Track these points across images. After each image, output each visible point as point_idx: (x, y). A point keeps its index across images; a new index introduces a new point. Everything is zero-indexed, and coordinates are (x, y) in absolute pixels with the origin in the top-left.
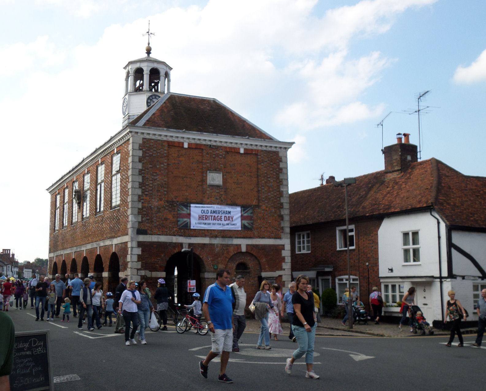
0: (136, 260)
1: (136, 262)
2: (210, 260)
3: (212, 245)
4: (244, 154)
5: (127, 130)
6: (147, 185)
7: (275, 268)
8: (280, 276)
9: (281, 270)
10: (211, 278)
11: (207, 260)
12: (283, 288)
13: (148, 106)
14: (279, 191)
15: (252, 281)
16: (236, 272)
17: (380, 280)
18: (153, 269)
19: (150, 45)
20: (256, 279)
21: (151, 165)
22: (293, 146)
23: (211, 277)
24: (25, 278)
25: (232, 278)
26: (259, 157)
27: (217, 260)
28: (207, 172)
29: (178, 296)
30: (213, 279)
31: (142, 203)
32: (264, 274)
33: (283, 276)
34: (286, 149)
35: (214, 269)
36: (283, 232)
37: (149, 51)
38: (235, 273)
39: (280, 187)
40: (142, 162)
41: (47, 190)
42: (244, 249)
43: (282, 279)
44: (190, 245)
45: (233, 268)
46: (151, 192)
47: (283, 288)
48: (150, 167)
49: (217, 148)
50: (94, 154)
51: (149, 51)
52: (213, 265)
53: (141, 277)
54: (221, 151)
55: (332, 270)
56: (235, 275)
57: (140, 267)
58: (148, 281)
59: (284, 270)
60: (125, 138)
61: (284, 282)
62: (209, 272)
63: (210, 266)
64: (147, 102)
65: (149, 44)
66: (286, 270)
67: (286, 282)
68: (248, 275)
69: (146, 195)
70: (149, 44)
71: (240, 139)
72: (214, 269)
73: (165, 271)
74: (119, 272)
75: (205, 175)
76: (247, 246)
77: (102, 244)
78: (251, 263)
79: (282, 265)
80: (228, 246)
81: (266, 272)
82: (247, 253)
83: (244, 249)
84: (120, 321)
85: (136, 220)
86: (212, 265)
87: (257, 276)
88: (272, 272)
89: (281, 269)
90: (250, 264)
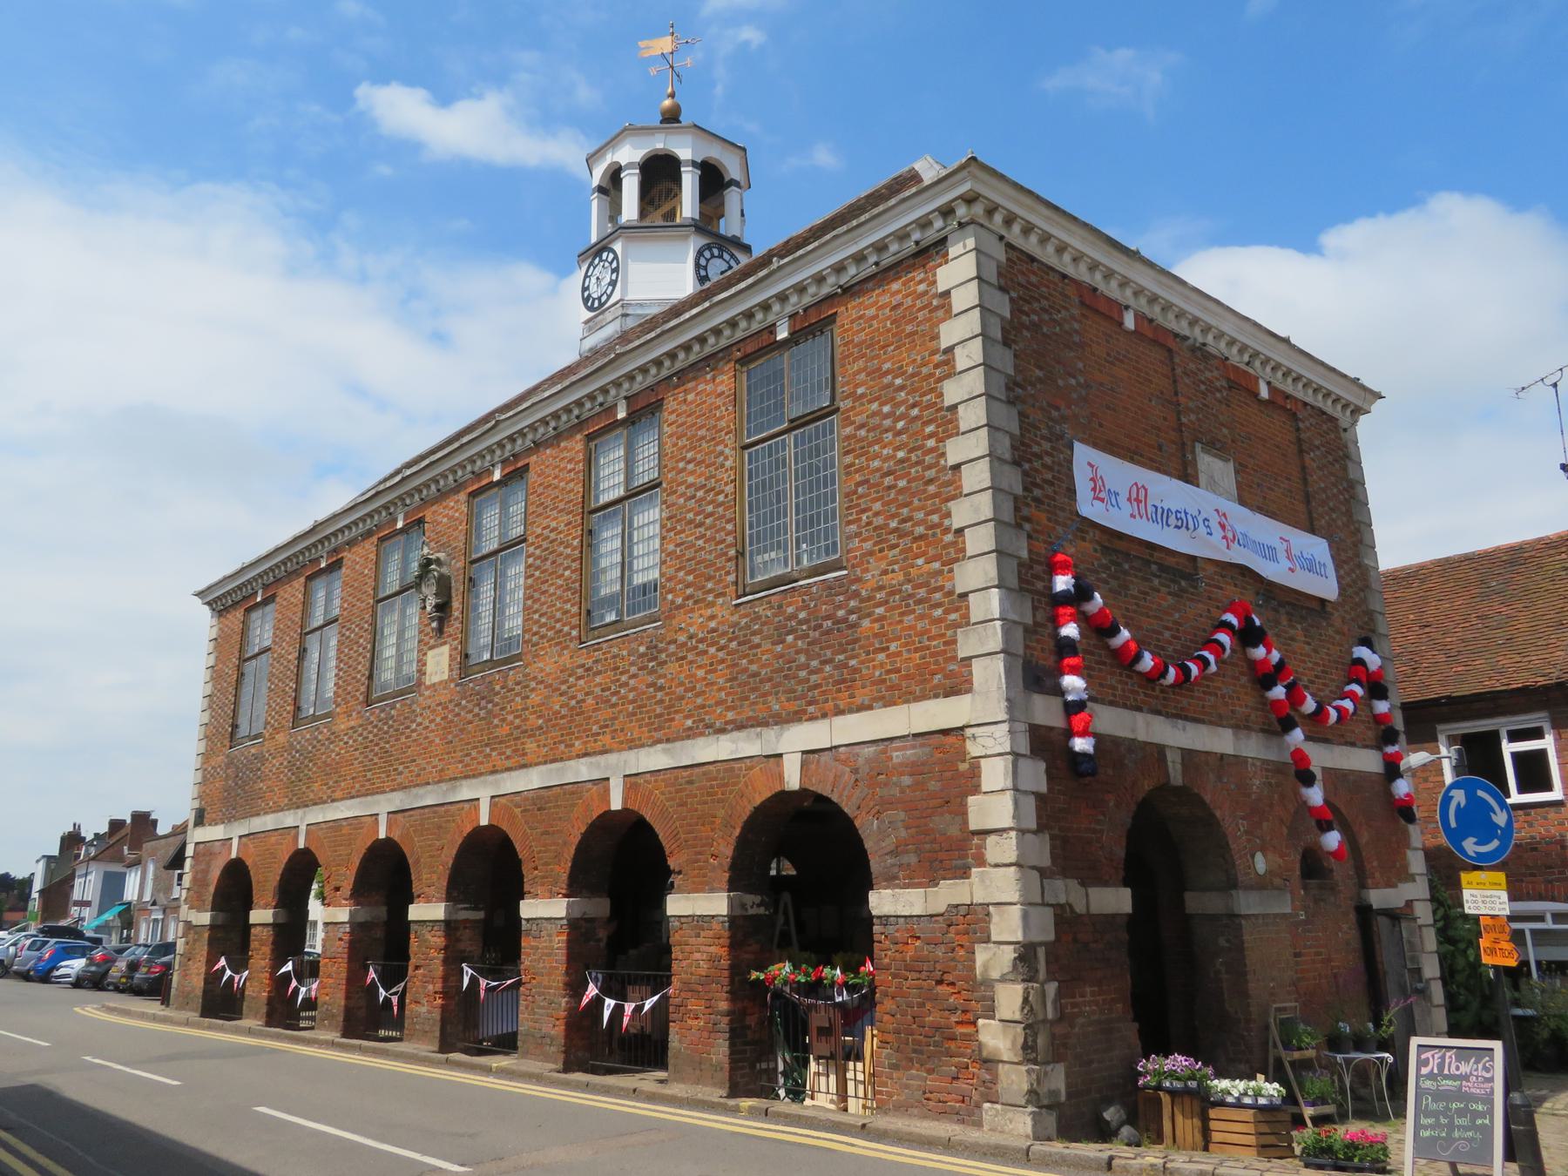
0: (1034, 826)
1: (1035, 832)
3: (1239, 760)
4: (1270, 403)
5: (963, 181)
6: (1038, 456)
13: (702, 279)
14: (1359, 566)
18: (1090, 876)
20: (1352, 916)
21: (1041, 368)
22: (1377, 406)
26: (1301, 425)
28: (1194, 447)
31: (1029, 537)
34: (1358, 411)
40: (1013, 346)
41: (199, 594)
46: (1049, 490)
48: (1040, 380)
50: (584, 386)
54: (1216, 373)
57: (1046, 861)
60: (350, 533)
64: (697, 266)
66: (1417, 878)
69: (1036, 500)
73: (1126, 885)
75: (1190, 457)
77: (654, 759)
84: (1457, 1083)
85: (1016, 618)
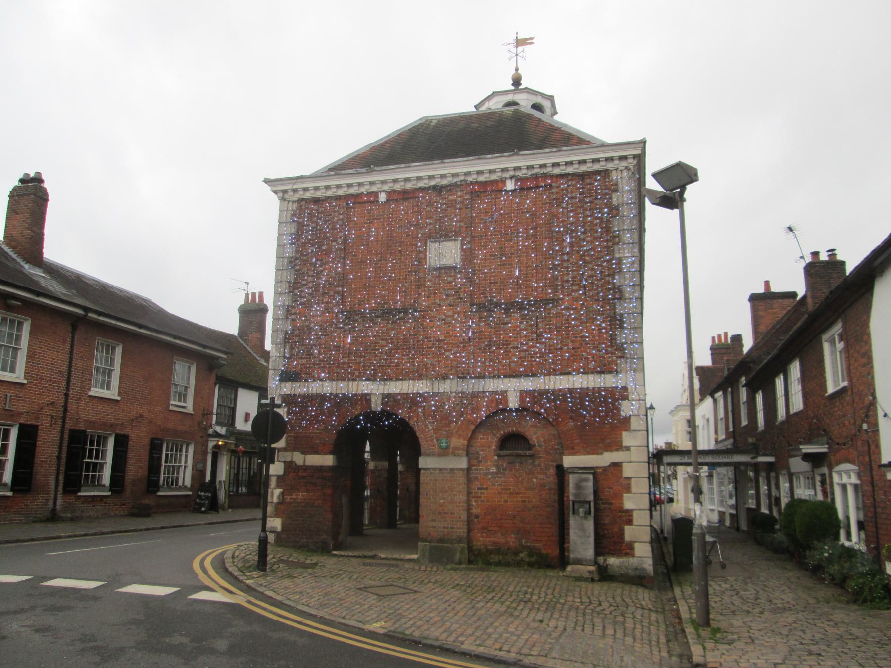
2: (430, 427)
7: (601, 445)
8: (617, 465)
9: (617, 450)
10: (434, 469)
11: (425, 431)
12: (625, 495)
15: (541, 476)
16: (499, 456)
17: (884, 475)
19: (519, 72)
23: (433, 467)
24: (271, 465)
25: (489, 469)
27: (448, 429)
29: (397, 506)
30: (437, 471)
32: (569, 461)
33: (624, 464)
35: (440, 447)
36: (621, 357)
37: (517, 82)
38: (496, 458)
39: (613, 251)
42: (513, 403)
43: (621, 471)
44: (386, 397)
45: (489, 447)
47: (625, 495)
49: (450, 188)
51: (517, 82)
52: (437, 440)
53: (285, 465)
55: (825, 450)
56: (496, 461)
58: (300, 473)
59: (628, 449)
61: (629, 479)
62: (428, 455)
63: (432, 441)
65: (517, 70)
67: (633, 480)
68: (530, 461)
70: (517, 70)
71: (496, 160)
72: (440, 447)
73: (331, 453)
74: (420, 455)
76: (523, 394)
78: (535, 433)
79: (621, 435)
80: (475, 396)
81: (574, 454)
82: (522, 410)
83: (513, 403)
86: (434, 441)
87: (555, 464)
88: (593, 454)
89: (618, 446)
90: (534, 437)
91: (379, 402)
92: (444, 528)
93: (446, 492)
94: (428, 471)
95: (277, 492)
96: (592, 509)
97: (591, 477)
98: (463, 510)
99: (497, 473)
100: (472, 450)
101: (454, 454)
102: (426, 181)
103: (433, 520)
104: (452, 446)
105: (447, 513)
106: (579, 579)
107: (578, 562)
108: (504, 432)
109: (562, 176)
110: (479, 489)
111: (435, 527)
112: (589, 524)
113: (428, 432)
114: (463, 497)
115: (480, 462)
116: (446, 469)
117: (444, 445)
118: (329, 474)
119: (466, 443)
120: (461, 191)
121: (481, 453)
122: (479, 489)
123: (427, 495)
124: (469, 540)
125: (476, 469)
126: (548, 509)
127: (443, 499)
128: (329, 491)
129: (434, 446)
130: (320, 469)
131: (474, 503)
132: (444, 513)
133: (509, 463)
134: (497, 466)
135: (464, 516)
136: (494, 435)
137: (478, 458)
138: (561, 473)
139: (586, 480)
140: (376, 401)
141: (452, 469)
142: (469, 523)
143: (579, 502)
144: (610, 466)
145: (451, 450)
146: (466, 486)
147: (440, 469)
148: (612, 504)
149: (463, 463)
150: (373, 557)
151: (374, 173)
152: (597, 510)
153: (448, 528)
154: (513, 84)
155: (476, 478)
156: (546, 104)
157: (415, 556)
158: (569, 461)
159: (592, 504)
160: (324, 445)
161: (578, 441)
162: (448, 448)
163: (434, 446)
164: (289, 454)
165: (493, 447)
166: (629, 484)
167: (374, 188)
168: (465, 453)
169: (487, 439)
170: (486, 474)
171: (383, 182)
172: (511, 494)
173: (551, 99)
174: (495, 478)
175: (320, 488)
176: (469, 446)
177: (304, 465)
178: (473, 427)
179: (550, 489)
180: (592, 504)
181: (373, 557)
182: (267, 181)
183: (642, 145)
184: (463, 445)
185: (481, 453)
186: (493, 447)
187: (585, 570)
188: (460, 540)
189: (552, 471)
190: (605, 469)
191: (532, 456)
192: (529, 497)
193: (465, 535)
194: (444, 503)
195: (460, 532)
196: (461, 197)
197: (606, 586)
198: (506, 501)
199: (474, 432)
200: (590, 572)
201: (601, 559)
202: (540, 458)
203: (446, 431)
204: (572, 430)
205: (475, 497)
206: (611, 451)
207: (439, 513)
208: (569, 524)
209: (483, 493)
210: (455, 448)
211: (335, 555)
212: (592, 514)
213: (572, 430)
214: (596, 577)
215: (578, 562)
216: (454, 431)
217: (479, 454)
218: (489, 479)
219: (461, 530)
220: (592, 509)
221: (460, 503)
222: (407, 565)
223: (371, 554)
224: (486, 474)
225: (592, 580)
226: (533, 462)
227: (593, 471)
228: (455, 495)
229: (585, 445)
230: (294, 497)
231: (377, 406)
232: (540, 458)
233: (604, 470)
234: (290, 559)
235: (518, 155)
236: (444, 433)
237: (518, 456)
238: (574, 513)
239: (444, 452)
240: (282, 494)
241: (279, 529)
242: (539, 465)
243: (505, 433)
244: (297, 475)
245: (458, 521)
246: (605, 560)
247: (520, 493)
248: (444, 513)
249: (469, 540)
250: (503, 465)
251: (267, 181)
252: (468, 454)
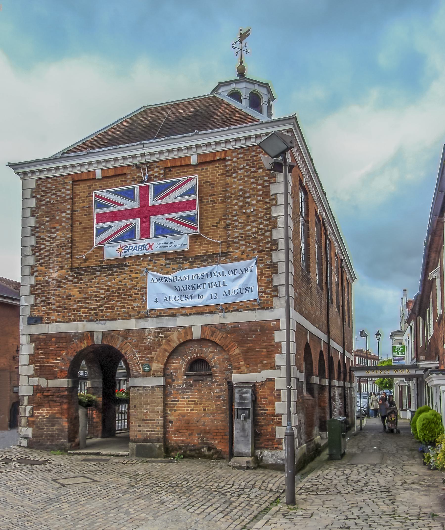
2: (137, 356)
8: (272, 380)
9: (271, 369)
10: (140, 387)
15: (217, 390)
32: (237, 378)
35: (144, 370)
37: (241, 73)
38: (185, 377)
45: (181, 369)
51: (241, 73)
52: (142, 365)
56: (185, 380)
62: (135, 377)
65: (241, 63)
68: (209, 379)
70: (241, 63)
76: (203, 327)
80: (168, 330)
86: (140, 365)
90: (212, 360)
91: (100, 337)
92: (147, 431)
93: (148, 404)
94: (136, 389)
95: (29, 408)
96: (251, 415)
97: (250, 390)
98: (161, 417)
99: (185, 389)
100: (168, 372)
101: (154, 376)
102: (121, 161)
103: (139, 426)
104: (152, 369)
105: (150, 420)
106: (240, 468)
107: (240, 455)
108: (191, 357)
109: (234, 150)
110: (173, 401)
111: (140, 431)
112: (248, 425)
113: (135, 359)
114: (160, 408)
115: (173, 381)
116: (148, 387)
117: (147, 368)
118: (66, 393)
119: (162, 366)
120: (157, 167)
121: (174, 374)
122: (173, 401)
123: (135, 406)
124: (165, 439)
125: (171, 386)
126: (222, 415)
127: (147, 409)
128: (65, 406)
129: (140, 369)
130: (58, 390)
131: (169, 412)
132: (147, 420)
133: (195, 381)
134: (186, 383)
135: (161, 422)
136: (184, 360)
137: (172, 378)
138: (231, 386)
139: (246, 393)
140: (97, 337)
141: (153, 387)
142: (165, 426)
143: (242, 409)
144: (266, 381)
145: (152, 372)
146: (162, 399)
147: (144, 387)
148: (267, 410)
149: (160, 381)
150: (98, 454)
151: (90, 155)
152: (255, 415)
153: (149, 431)
154: (238, 75)
155: (171, 393)
156: (263, 91)
157: (127, 453)
158: (237, 378)
159: (251, 410)
160: (61, 371)
161: (243, 363)
162: (150, 370)
163: (140, 369)
164: (37, 379)
165: (183, 369)
166: (280, 395)
167: (92, 168)
168: (162, 374)
169: (179, 363)
170: (178, 390)
171: (98, 162)
172: (196, 404)
173: (266, 86)
174: (184, 392)
175: (59, 404)
176: (165, 369)
177: (47, 387)
178: (167, 354)
179: (224, 400)
180: (251, 410)
181: (98, 454)
182: (10, 165)
183: (293, 120)
184: (161, 368)
185: (174, 374)
186: (183, 369)
187: (243, 461)
188: (158, 440)
189: (225, 386)
190: (263, 384)
191: (211, 375)
192: (208, 407)
193: (162, 436)
194: (147, 412)
195: (158, 434)
196: (157, 172)
197: (260, 471)
198: (192, 410)
199: (169, 358)
200: (247, 462)
201: (258, 452)
202: (217, 376)
203: (148, 358)
204: (240, 354)
205: (170, 407)
206: (267, 369)
207: (144, 420)
208: (229, 428)
209: (176, 404)
210: (155, 371)
211: (70, 453)
212: (251, 418)
213: (240, 354)
214: (252, 465)
215: (240, 455)
216: (154, 358)
217: (173, 375)
218: (180, 393)
219: (159, 432)
220: (251, 415)
221: (158, 412)
222: (121, 460)
223: (95, 451)
224: (178, 390)
225: (248, 468)
226: (212, 380)
227: (254, 386)
228: (155, 406)
229: (248, 366)
230: (40, 411)
231: (98, 340)
232: (217, 376)
233: (262, 385)
234: (382, 379)
235: (197, 134)
236: (147, 359)
237: (201, 375)
238: (237, 418)
239: (147, 374)
240: (32, 409)
241: (30, 436)
242: (216, 382)
243: (189, 360)
244: (43, 395)
245: (157, 426)
246: (261, 453)
247: (202, 404)
248: (147, 420)
249: (165, 439)
250: (190, 383)
251: (10, 165)
252: (164, 375)
